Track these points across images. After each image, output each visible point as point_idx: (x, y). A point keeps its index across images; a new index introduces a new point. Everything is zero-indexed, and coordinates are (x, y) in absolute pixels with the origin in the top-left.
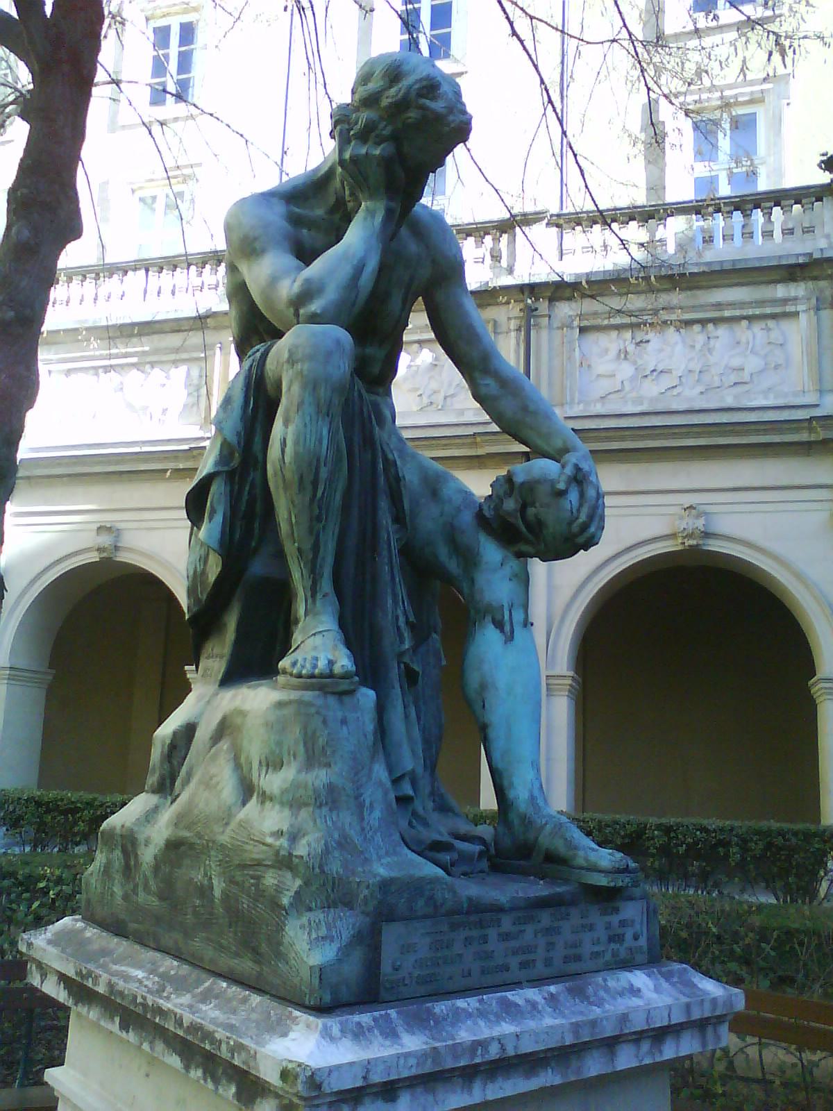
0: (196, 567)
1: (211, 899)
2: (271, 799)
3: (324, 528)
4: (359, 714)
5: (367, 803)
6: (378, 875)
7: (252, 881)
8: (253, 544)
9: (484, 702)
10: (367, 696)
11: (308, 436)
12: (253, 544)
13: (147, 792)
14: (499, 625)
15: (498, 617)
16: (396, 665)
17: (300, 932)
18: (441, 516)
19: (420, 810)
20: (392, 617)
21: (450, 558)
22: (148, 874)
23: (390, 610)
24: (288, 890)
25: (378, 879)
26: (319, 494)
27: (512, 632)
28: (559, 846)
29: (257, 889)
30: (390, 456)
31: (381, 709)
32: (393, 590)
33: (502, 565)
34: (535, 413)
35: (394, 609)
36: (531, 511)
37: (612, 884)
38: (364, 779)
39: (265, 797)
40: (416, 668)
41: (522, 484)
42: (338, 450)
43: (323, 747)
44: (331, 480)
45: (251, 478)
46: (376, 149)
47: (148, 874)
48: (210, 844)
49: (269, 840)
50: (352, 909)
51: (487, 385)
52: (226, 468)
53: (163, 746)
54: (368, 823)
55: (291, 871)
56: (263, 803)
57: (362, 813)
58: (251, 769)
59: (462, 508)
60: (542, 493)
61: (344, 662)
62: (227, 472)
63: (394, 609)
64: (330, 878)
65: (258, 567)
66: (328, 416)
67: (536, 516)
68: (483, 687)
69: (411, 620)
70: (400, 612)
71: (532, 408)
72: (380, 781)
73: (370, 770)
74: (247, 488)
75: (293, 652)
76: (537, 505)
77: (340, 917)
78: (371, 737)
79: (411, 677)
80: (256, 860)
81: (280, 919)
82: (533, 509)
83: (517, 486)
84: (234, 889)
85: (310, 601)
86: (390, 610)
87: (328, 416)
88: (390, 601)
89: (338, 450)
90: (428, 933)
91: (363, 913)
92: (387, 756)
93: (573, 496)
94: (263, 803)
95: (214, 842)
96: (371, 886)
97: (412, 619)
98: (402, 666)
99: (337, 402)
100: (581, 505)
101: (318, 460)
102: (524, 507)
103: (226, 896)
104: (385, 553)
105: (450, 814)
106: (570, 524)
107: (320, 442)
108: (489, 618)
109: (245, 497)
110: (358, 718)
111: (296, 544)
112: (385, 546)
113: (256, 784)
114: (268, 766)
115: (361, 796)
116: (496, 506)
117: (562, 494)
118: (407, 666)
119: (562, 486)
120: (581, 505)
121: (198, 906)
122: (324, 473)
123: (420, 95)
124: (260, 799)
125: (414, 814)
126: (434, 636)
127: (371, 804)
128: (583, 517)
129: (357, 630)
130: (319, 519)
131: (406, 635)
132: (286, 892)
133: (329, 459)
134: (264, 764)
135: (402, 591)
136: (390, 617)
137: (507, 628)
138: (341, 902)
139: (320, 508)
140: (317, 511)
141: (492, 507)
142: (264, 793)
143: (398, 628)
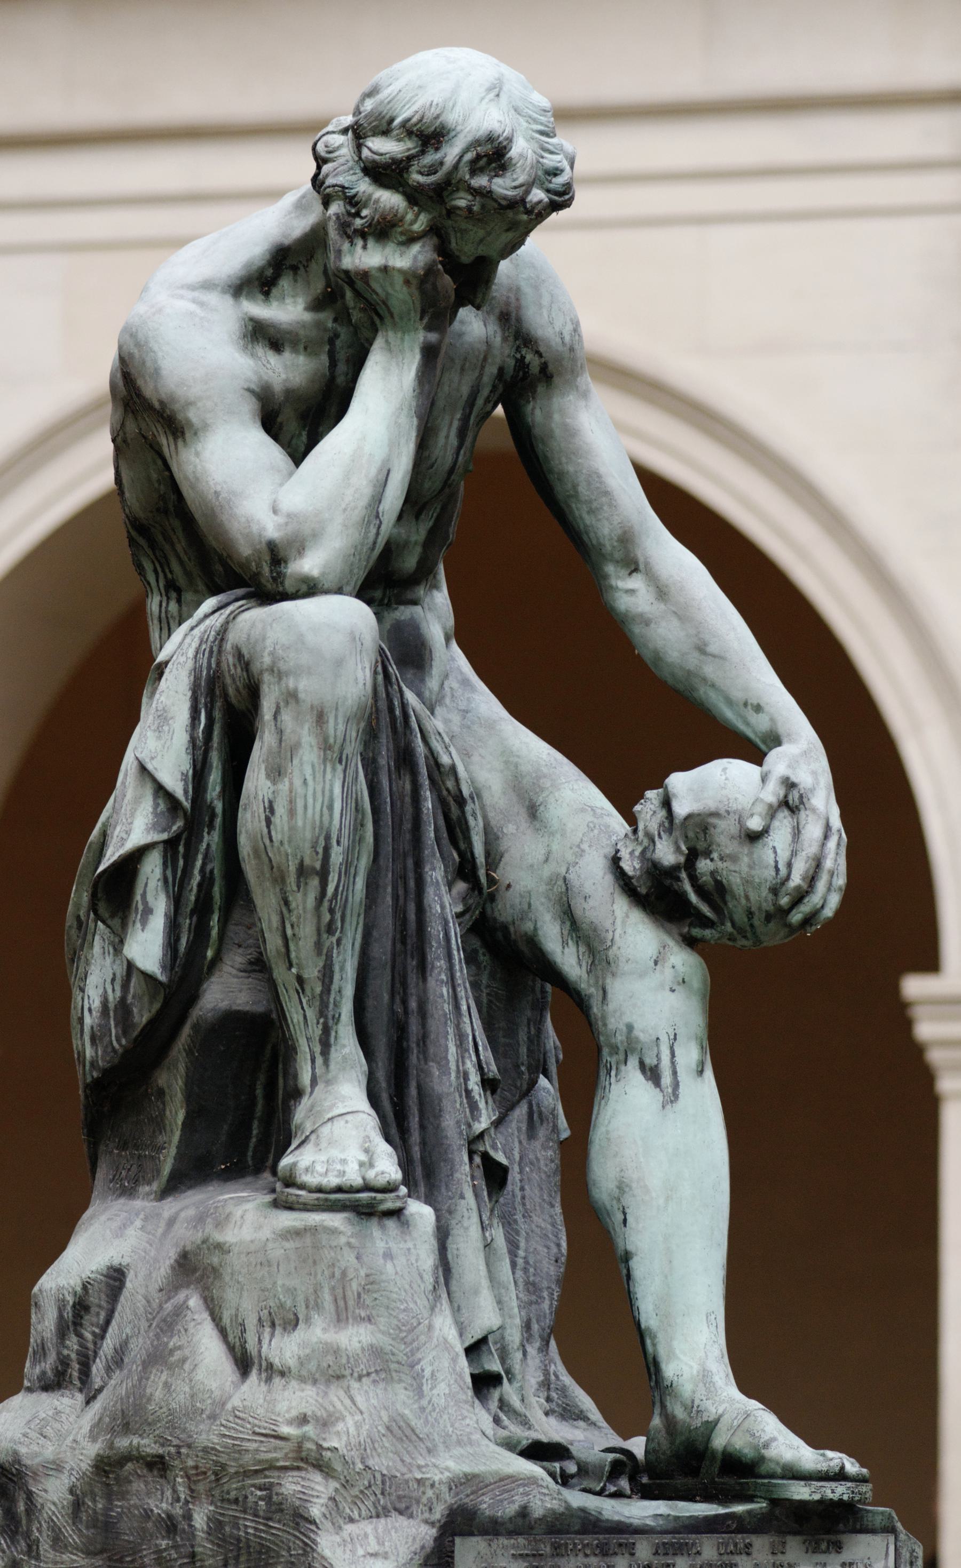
0: (105, 991)
1: (191, 1534)
2: (282, 1374)
3: (339, 942)
4: (410, 1245)
5: (427, 1373)
6: (447, 1469)
7: (259, 1493)
8: (210, 954)
9: (625, 1214)
10: (421, 1212)
11: (310, 801)
12: (210, 954)
13: (30, 1390)
14: (652, 1074)
15: (650, 1061)
16: (466, 1158)
17: (339, 1551)
18: (547, 860)
19: (515, 1401)
20: (458, 1078)
21: (564, 944)
22: (61, 1520)
23: (453, 1066)
24: (318, 1497)
25: (447, 1474)
26: (331, 889)
27: (676, 1085)
28: (740, 1443)
29: (268, 1499)
30: (445, 759)
31: (443, 1234)
32: (458, 1026)
33: (656, 963)
34: (719, 658)
35: (459, 1053)
36: (704, 865)
37: (817, 1497)
38: (423, 1338)
39: (271, 1371)
40: (500, 1157)
41: (689, 817)
42: (358, 809)
43: (359, 1295)
44: (348, 866)
45: (204, 845)
46: (421, 1216)
47: (61, 1520)
48: (183, 1450)
49: (285, 1430)
50: (411, 1516)
51: (631, 592)
52: (165, 836)
53: (60, 1311)
54: (429, 1402)
55: (321, 1471)
56: (269, 1380)
57: (420, 1386)
58: (244, 1331)
59: (585, 846)
60: (724, 832)
61: (387, 1167)
62: (165, 842)
63: (459, 1053)
64: (378, 1476)
65: (225, 992)
66: (340, 762)
67: (713, 873)
68: (622, 1187)
69: (491, 1075)
70: (471, 1066)
71: (712, 649)
72: (446, 1340)
73: (430, 1327)
74: (199, 863)
75: (296, 1148)
76: (715, 855)
77: (394, 1527)
78: (429, 1279)
79: (495, 1176)
80: (267, 1461)
81: (309, 1538)
82: (708, 861)
83: (677, 821)
84: (232, 1511)
85: (319, 1060)
86: (453, 1066)
87: (340, 762)
88: (452, 1049)
89: (358, 809)
90: (521, 1555)
91: (426, 1522)
92: (456, 1311)
93: (780, 837)
94: (269, 1380)
95: (189, 1446)
96: (437, 1485)
97: (493, 1069)
98: (478, 1160)
99: (354, 734)
100: (794, 853)
101: (328, 838)
102: (693, 855)
103: (216, 1526)
104: (441, 963)
105: (581, 1423)
106: (775, 891)
107: (331, 808)
108: (633, 1062)
109: (196, 878)
110: (409, 1249)
111: (294, 970)
112: (441, 952)
113: (254, 1353)
114: (273, 1325)
115: (418, 1363)
116: (643, 853)
117: (754, 837)
118: (486, 1157)
119: (755, 824)
120: (794, 853)
121: (165, 1550)
122: (337, 856)
123: (476, 167)
124: (264, 1375)
125: (503, 1404)
126: (543, 1081)
127: (433, 1374)
128: (796, 879)
129: (400, 1105)
130: (330, 929)
131: (482, 1105)
132: (315, 1500)
133: (345, 832)
134: (267, 1324)
135: (473, 1025)
136: (453, 1075)
137: (666, 1079)
138: (395, 1509)
139: (331, 911)
140: (327, 917)
141: (637, 853)
142: (270, 1366)
143: (468, 1092)
